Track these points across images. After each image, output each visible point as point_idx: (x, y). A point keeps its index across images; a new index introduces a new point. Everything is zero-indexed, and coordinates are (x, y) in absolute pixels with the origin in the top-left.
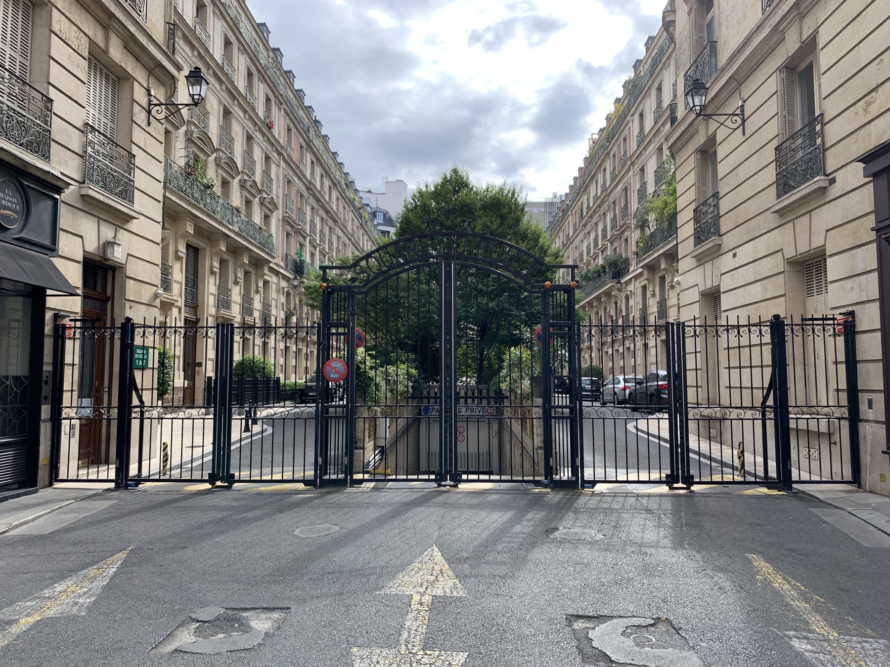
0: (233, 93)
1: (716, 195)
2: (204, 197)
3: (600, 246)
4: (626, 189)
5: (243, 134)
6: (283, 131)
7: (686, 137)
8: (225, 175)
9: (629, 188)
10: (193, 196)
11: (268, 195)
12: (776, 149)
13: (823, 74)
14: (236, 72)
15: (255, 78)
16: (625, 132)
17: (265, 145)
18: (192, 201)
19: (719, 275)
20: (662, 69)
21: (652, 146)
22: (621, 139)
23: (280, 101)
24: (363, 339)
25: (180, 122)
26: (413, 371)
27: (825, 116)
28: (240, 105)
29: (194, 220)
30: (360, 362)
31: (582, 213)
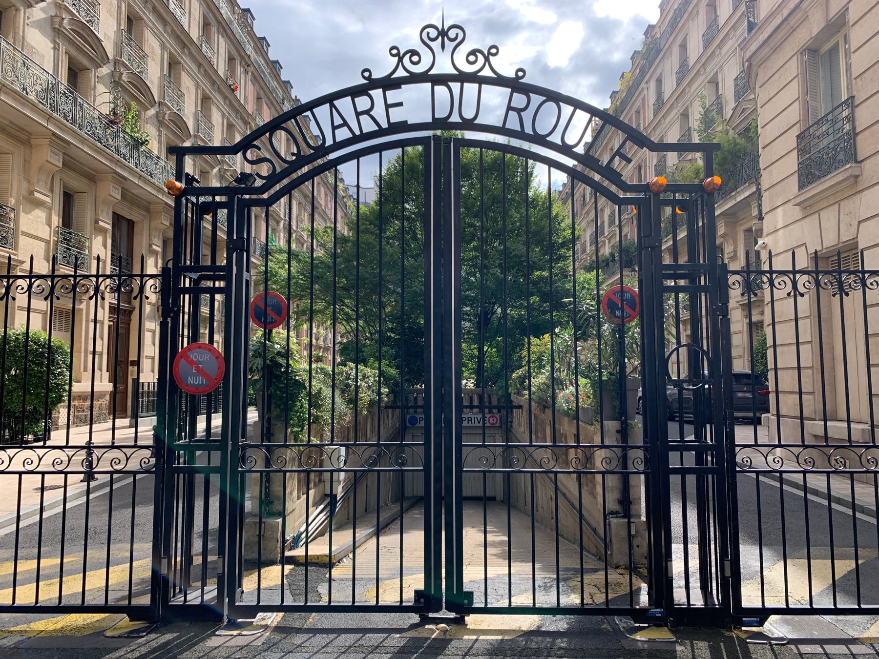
0: (181, 38)
1: (851, 102)
2: (136, 154)
3: (606, 234)
4: (639, 167)
5: (197, 91)
6: (251, 98)
7: (780, 35)
8: (74, 52)
9: (643, 165)
10: (118, 151)
11: (231, 167)
12: (798, 136)
13: (854, 52)
14: (216, 55)
15: (214, 29)
16: (639, 103)
17: (226, 109)
18: (116, 156)
19: (856, 223)
20: (687, 20)
21: (675, 112)
22: (633, 111)
23: (246, 63)
24: (285, 312)
25: (102, 58)
26: (393, 371)
27: (856, 98)
28: (191, 55)
29: (121, 183)
30: (279, 353)
31: (584, 199)
